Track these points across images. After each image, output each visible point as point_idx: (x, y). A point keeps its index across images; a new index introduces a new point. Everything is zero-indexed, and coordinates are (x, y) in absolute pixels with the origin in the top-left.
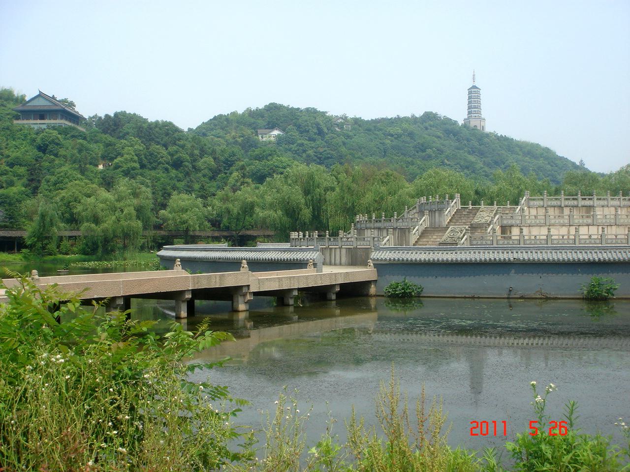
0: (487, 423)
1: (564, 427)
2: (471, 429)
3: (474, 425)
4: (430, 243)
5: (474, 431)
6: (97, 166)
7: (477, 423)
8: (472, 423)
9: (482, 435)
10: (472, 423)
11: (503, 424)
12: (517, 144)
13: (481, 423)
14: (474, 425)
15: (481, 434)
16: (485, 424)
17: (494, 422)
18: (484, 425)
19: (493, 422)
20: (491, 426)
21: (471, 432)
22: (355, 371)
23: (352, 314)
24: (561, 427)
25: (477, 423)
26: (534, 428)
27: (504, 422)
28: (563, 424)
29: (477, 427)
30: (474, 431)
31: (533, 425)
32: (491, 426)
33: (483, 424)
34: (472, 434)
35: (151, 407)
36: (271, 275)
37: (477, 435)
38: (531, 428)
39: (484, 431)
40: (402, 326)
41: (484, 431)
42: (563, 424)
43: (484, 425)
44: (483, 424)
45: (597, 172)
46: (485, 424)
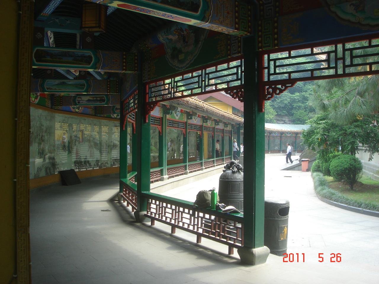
0: (293, 255)
1: (339, 257)
2: (331, 258)
3: (333, 256)
5: (333, 259)
8: (331, 254)
10: (331, 254)
12: (50, 158)
13: (290, 255)
14: (333, 256)
17: (298, 254)
18: (291, 256)
19: (297, 254)
20: (295, 257)
22: (316, 167)
24: (337, 257)
25: (335, 255)
27: (303, 254)
28: (339, 255)
30: (333, 259)
31: (321, 256)
32: (295, 257)
38: (319, 257)
39: (291, 260)
41: (291, 260)
42: (339, 255)
43: (291, 256)
45: (30, 232)
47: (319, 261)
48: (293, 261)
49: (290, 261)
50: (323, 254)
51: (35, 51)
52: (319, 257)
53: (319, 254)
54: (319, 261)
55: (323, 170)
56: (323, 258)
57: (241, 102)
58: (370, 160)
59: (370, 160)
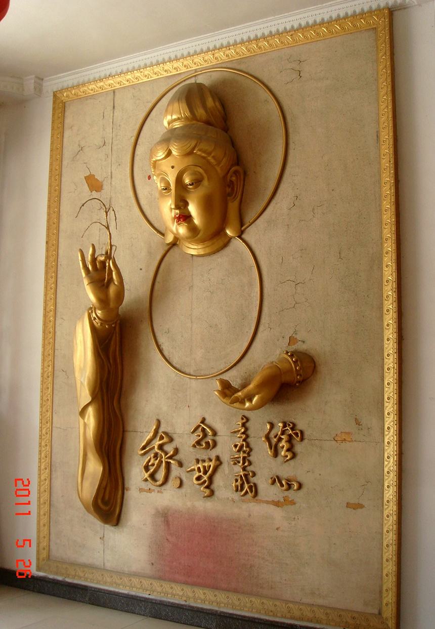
0: (28, 496)
2: (23, 560)
3: (26, 483)
4: (82, 380)
5: (19, 483)
6: (244, 404)
7: (28, 486)
9: (15, 490)
11: (28, 512)
13: (28, 490)
16: (27, 494)
17: (29, 503)
18: (26, 493)
19: (29, 502)
20: (25, 500)
21: (20, 560)
23: (94, 416)
26: (24, 544)
29: (24, 486)
30: (19, 483)
31: (27, 543)
33: (27, 491)
35: (244, 270)
36: (78, 341)
37: (16, 486)
38: (24, 541)
39: (19, 493)
40: (114, 490)
41: (19, 493)
43: (26, 493)
44: (27, 491)
46: (27, 494)
47: (18, 540)
49: (17, 490)
50: (30, 546)
51: (145, 451)
52: (24, 541)
53: (30, 541)
55: (122, 251)
56: (23, 546)
57: (94, 175)
58: (361, 424)
59: (361, 424)
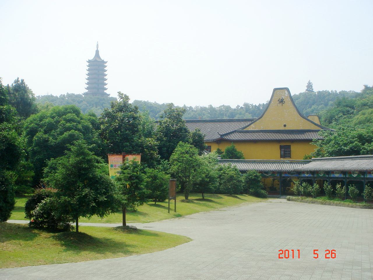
1: (334, 253)
15: (332, 257)
18: (287, 252)
24: (332, 253)
28: (333, 252)
34: (326, 258)
38: (314, 254)
39: (287, 256)
41: (287, 256)
43: (287, 252)
47: (314, 257)
48: (335, 257)
52: (314, 254)
53: (314, 250)
54: (314, 257)
